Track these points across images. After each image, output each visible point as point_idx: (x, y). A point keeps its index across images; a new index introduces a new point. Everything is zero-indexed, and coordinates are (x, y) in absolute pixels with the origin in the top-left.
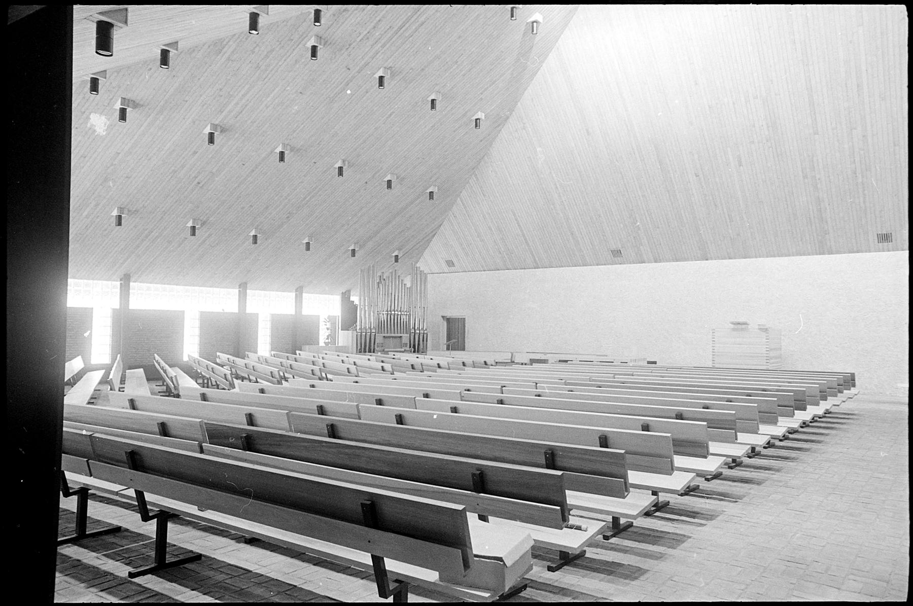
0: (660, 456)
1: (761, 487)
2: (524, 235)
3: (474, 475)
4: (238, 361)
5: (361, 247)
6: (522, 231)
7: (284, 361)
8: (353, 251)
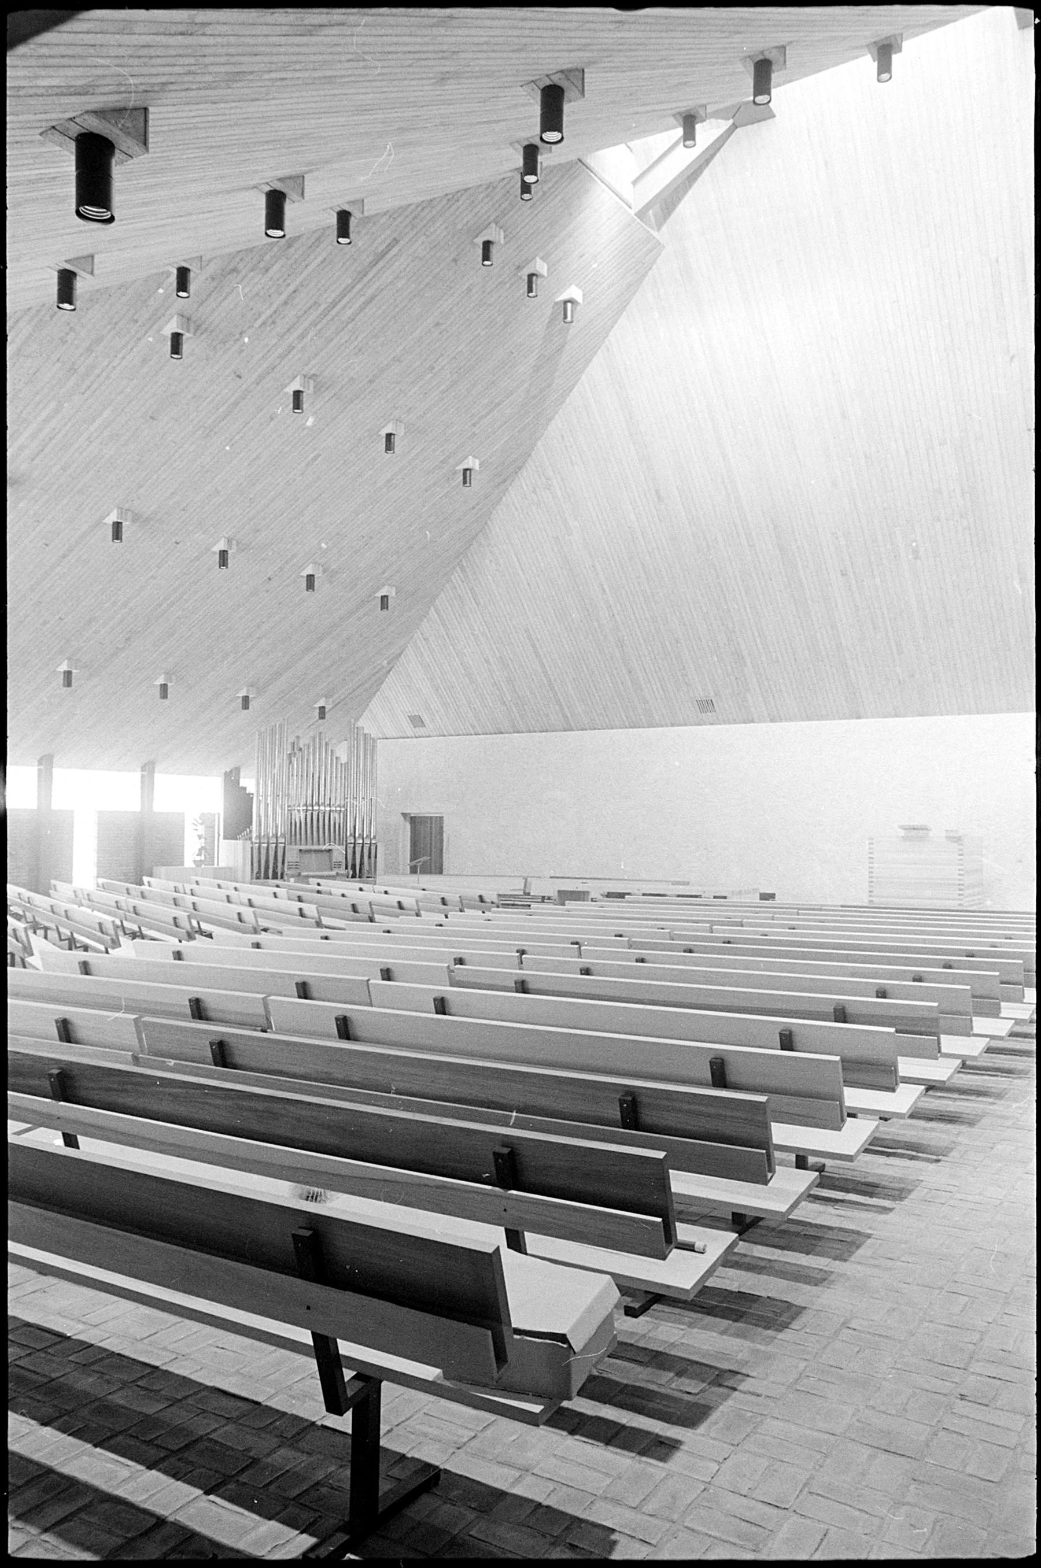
0: (818, 1096)
1: (975, 1130)
2: (545, 672)
3: (497, 1155)
4: (38, 898)
5: (260, 691)
6: (543, 665)
7: (122, 898)
8: (246, 701)
